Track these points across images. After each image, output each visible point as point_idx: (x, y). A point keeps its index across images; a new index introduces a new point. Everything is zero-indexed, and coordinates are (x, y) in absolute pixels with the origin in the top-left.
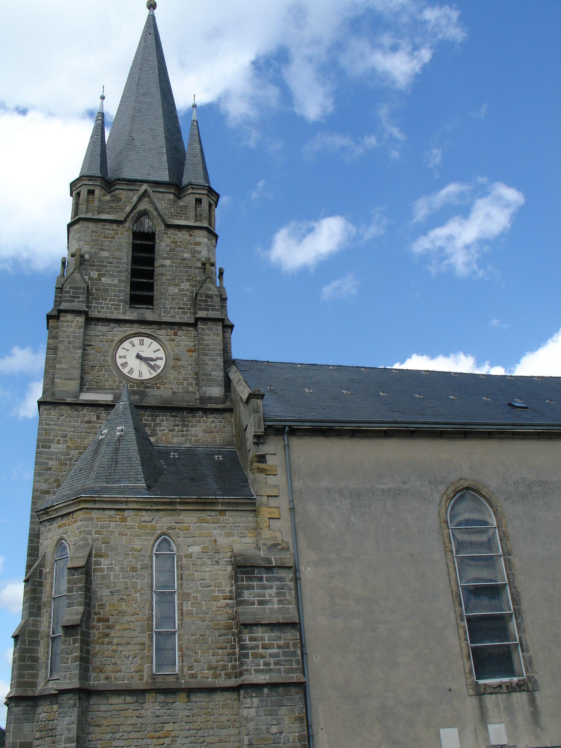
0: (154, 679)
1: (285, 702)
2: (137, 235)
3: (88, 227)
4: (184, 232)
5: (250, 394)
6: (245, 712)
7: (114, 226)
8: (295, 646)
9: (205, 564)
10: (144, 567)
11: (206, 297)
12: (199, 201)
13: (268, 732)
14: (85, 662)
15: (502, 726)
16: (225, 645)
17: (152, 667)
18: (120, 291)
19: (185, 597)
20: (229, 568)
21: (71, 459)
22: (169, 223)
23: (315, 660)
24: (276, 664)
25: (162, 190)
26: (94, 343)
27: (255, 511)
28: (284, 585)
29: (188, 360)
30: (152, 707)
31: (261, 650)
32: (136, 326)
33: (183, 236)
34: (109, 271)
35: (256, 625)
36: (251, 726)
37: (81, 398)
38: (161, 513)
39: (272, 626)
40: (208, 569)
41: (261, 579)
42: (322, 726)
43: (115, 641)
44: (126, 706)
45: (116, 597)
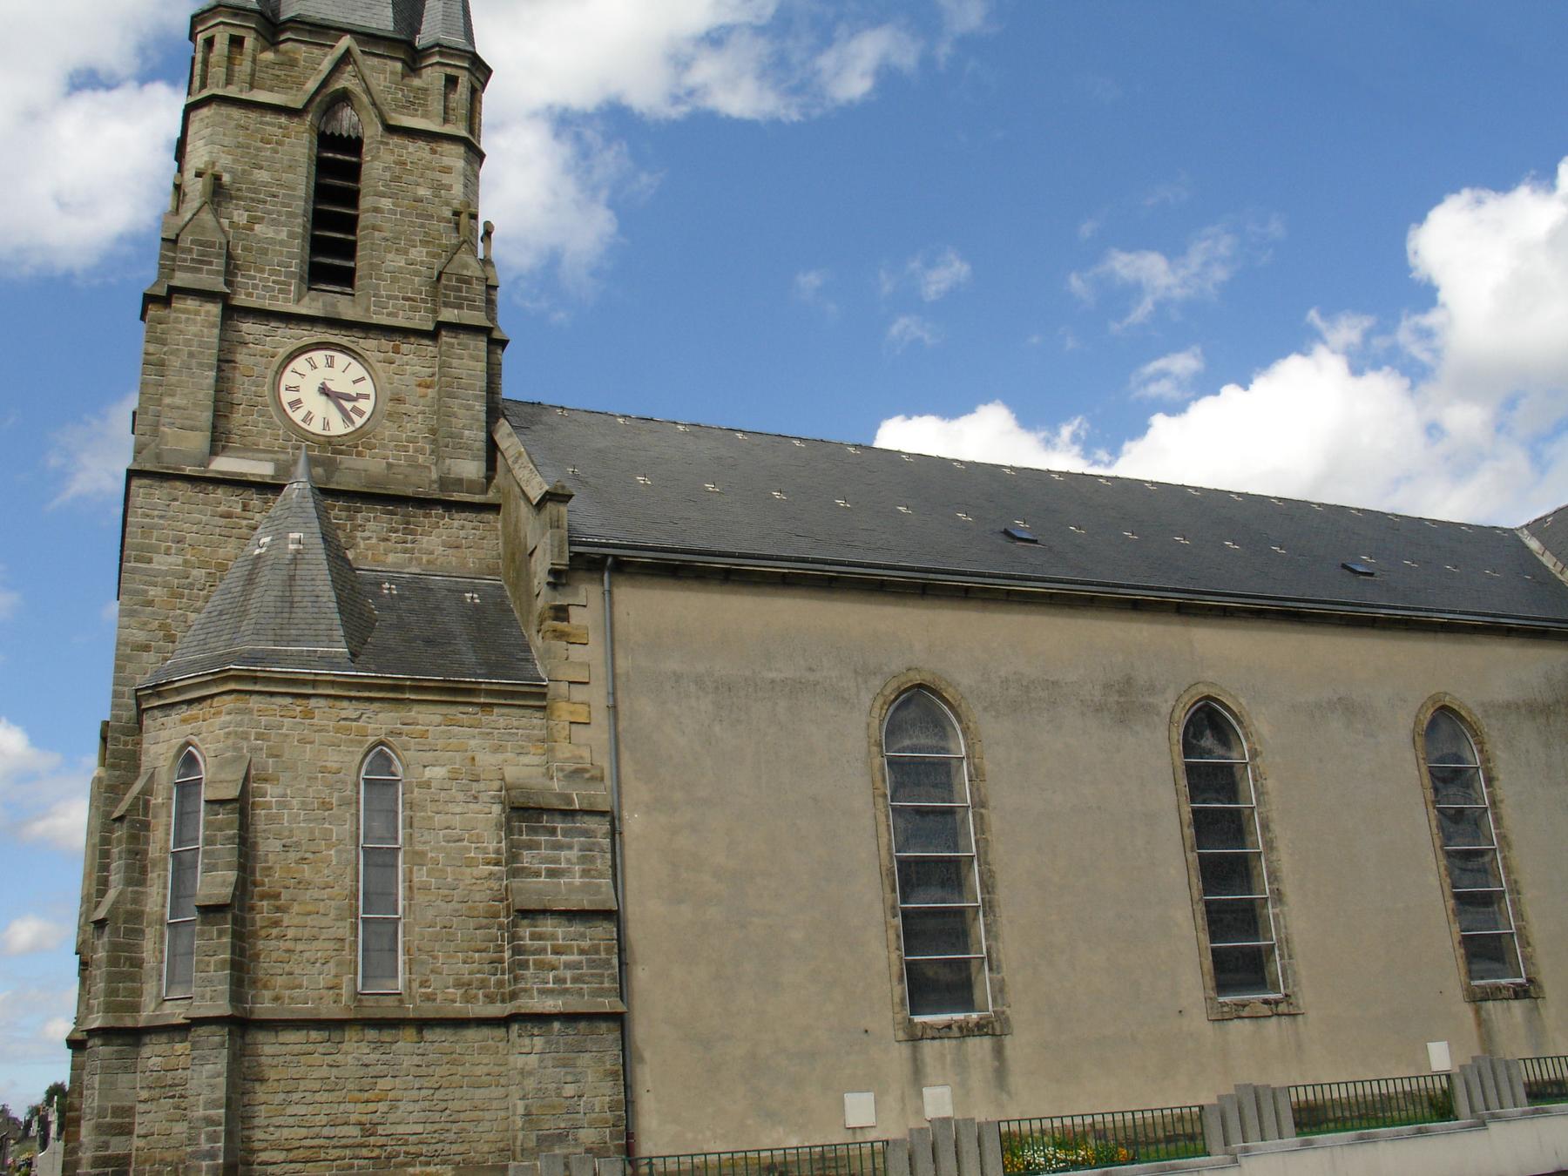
1: (589, 1046)
2: (326, 140)
3: (229, 117)
4: (421, 143)
5: (547, 492)
6: (520, 1061)
7: (283, 120)
8: (608, 950)
10: (344, 803)
11: (458, 280)
13: (559, 1095)
15: (946, 1090)
17: (355, 981)
19: (417, 858)
20: (496, 809)
21: (191, 586)
22: (392, 123)
23: (641, 975)
24: (575, 980)
27: (543, 708)
29: (419, 403)
30: (356, 1049)
31: (550, 957)
33: (417, 151)
35: (544, 912)
36: (530, 1083)
39: (571, 915)
40: (458, 810)
41: (553, 832)
42: (649, 1085)
43: (291, 933)
44: (311, 1048)
45: (293, 856)
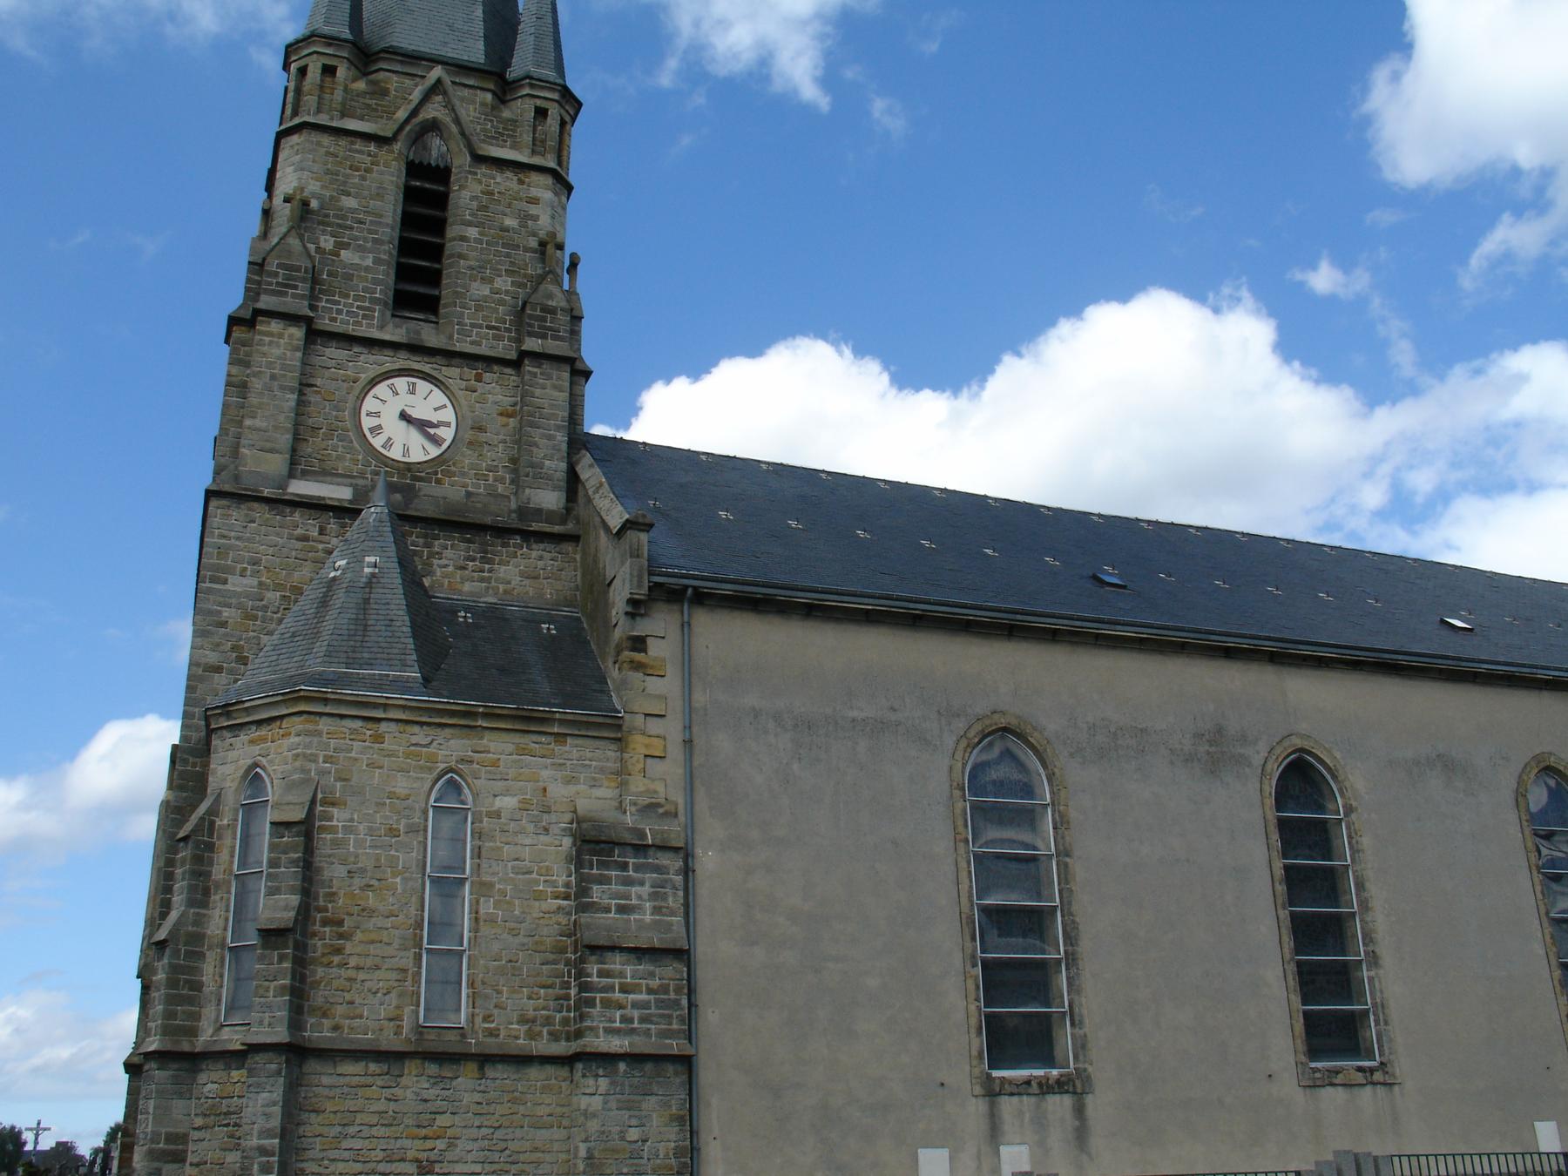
0: (421, 1033)
1: (655, 1088)
2: (415, 169)
3: (319, 144)
4: (509, 174)
6: (584, 1102)
7: (372, 148)
8: (678, 990)
9: (522, 832)
10: (411, 829)
12: (541, 113)
13: (623, 1139)
14: (299, 995)
16: (550, 981)
17: (417, 1013)
18: (376, 282)
19: (483, 889)
20: (567, 842)
23: (711, 1018)
24: (643, 1020)
25: (471, 82)
26: (318, 382)
27: (619, 740)
28: (666, 881)
29: (499, 432)
30: (415, 1083)
31: (617, 995)
32: (403, 354)
33: (505, 182)
34: (356, 239)
35: (612, 948)
36: (593, 1126)
37: (290, 490)
38: (448, 731)
39: (640, 953)
40: (528, 841)
41: (624, 867)
42: (716, 1132)
43: (353, 962)
44: (369, 1080)
45: (357, 882)
